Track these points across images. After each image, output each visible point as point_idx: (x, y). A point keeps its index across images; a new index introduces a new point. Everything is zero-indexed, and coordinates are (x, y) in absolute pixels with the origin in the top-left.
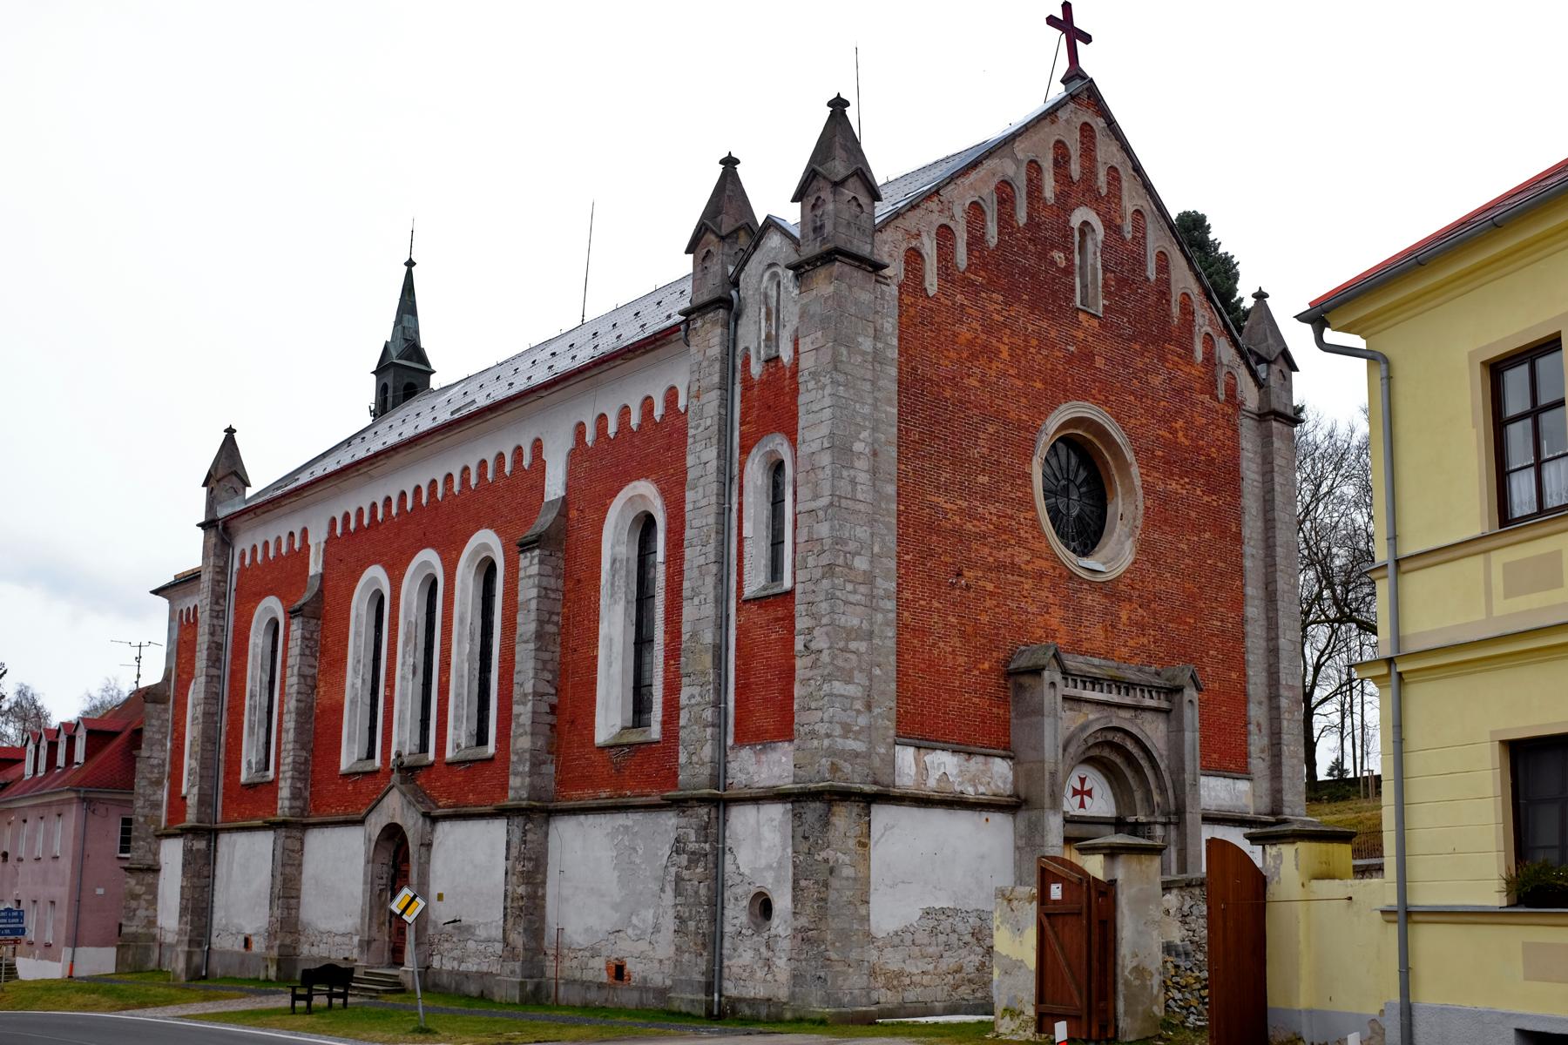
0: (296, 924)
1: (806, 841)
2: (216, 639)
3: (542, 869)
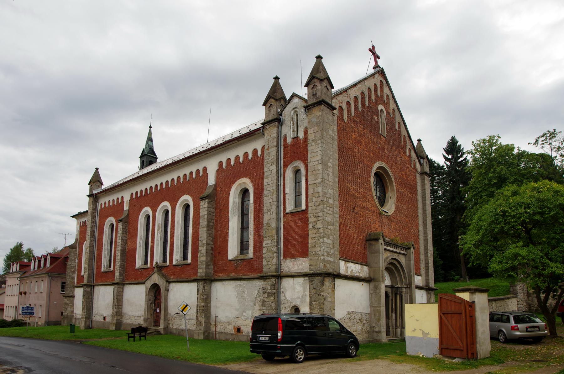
2: (93, 229)
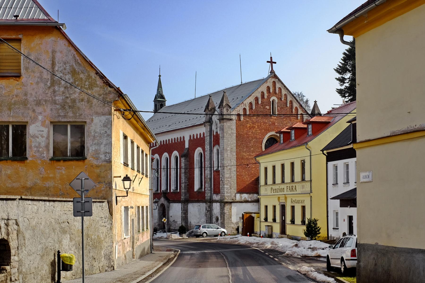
1: (222, 209)
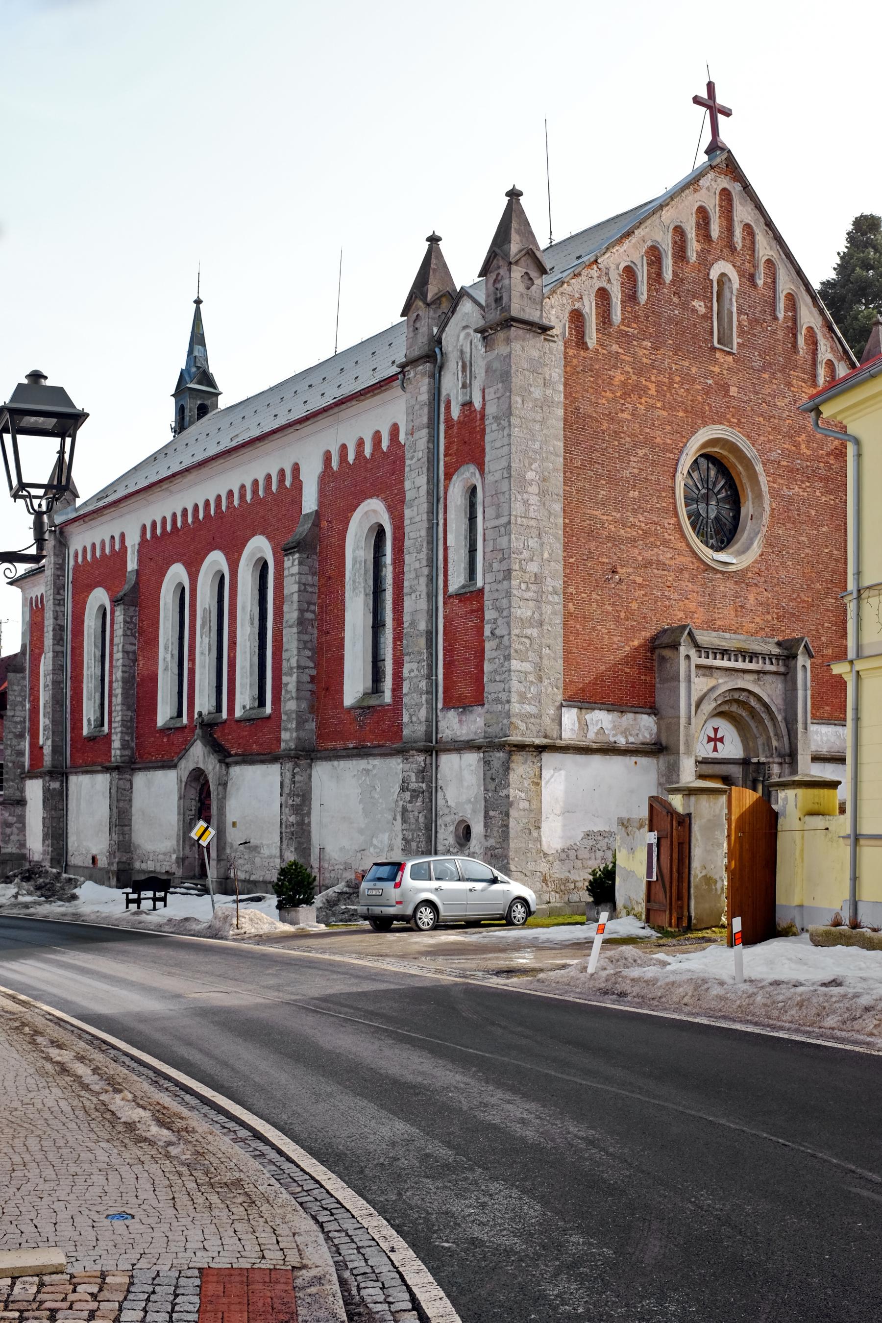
0: (130, 846)
2: (59, 622)
3: (307, 803)
